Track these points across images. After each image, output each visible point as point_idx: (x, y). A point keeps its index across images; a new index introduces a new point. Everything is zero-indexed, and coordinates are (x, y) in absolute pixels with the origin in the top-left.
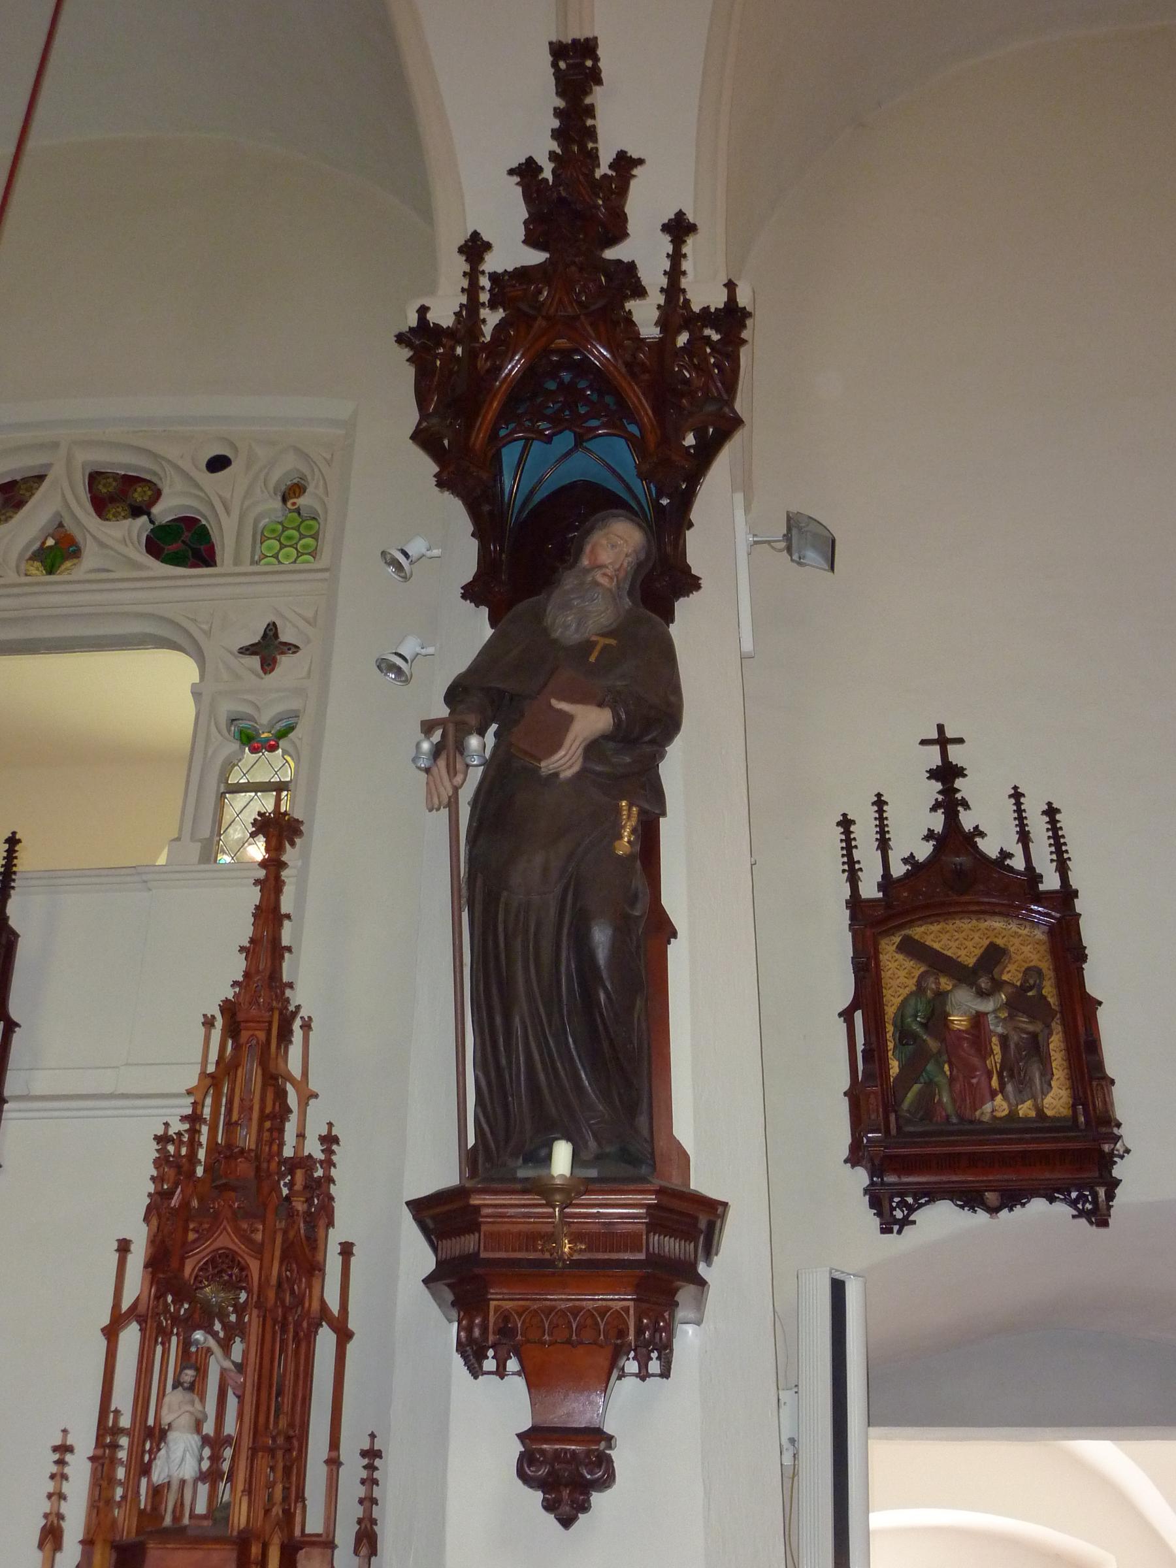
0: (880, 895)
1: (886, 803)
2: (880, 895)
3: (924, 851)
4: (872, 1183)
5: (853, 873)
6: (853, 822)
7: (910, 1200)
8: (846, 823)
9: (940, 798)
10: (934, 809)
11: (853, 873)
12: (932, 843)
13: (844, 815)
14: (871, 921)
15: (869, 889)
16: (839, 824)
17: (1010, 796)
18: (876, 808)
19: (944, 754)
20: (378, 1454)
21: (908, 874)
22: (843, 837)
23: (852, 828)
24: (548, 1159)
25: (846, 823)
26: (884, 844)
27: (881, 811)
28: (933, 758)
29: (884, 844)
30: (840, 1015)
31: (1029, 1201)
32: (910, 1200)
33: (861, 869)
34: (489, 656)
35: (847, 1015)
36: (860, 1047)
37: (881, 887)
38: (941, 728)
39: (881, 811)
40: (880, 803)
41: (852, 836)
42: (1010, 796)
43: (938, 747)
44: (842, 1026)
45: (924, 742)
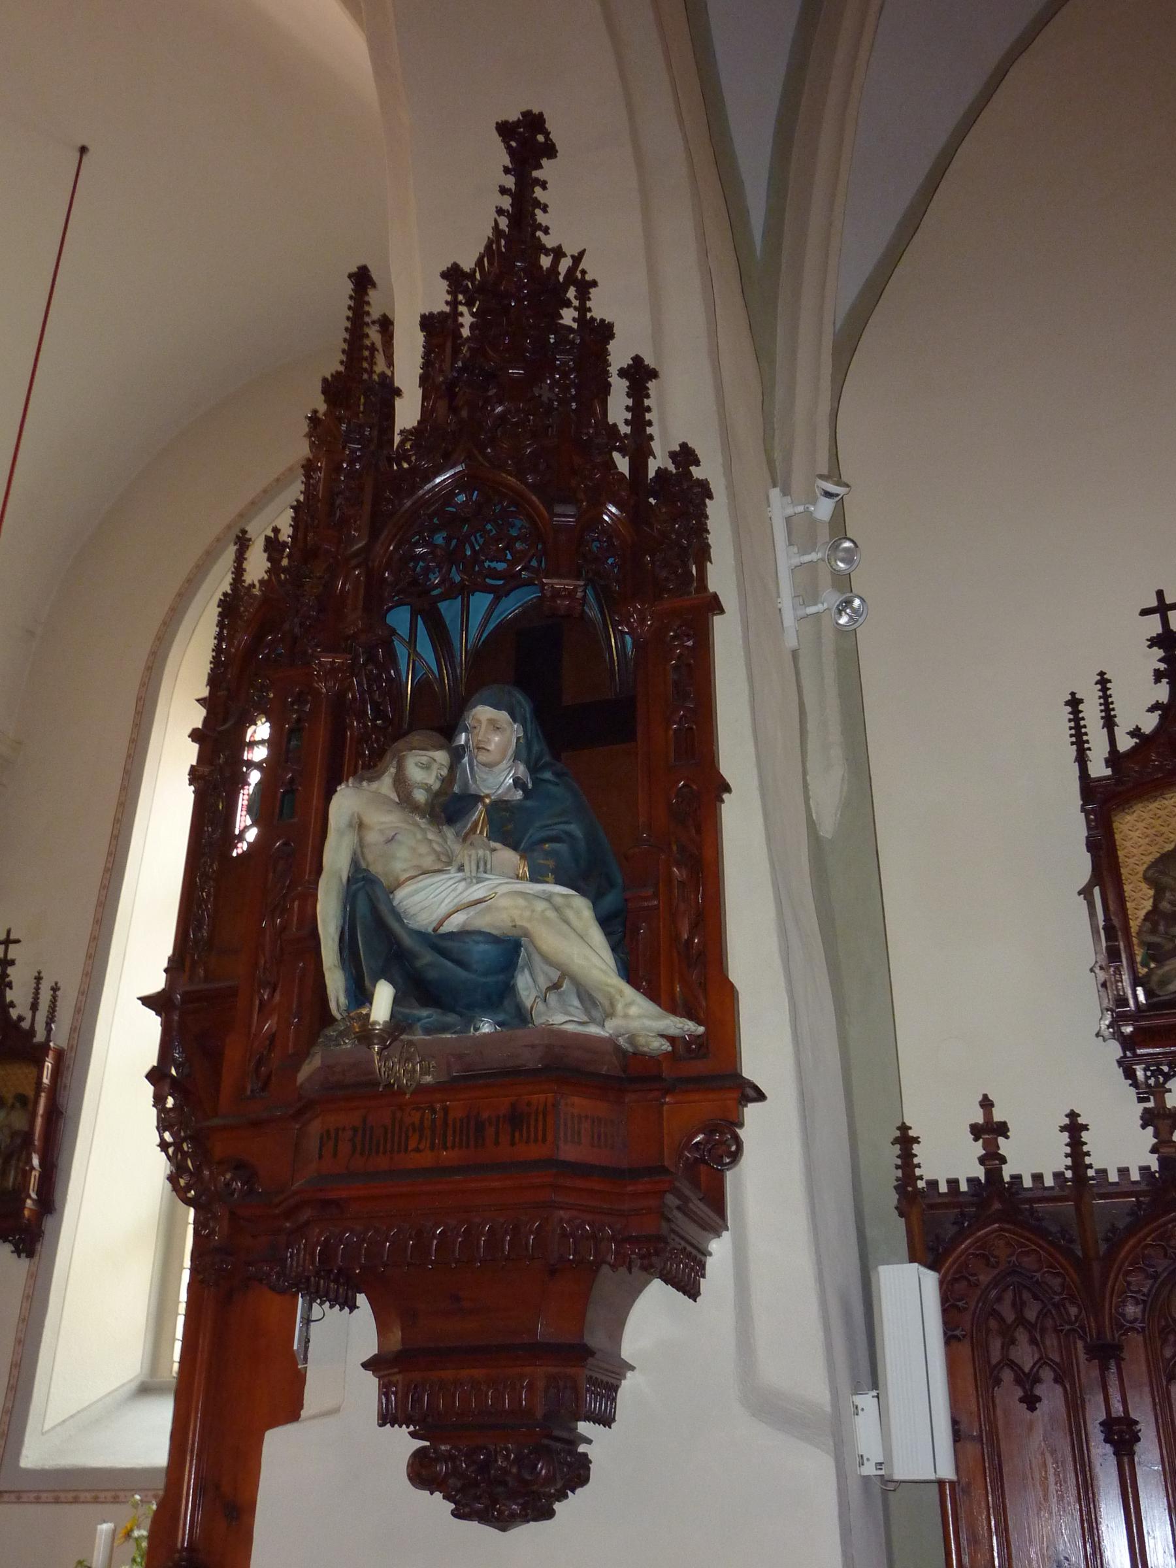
0: (1109, 772)
1: (1110, 681)
2: (1109, 772)
3: (1150, 723)
4: (1125, 1056)
5: (1082, 759)
6: (1081, 701)
7: (1166, 1069)
8: (1074, 703)
9: (1162, 666)
10: (1151, 709)
11: (1082, 759)
12: (1165, 681)
13: (1073, 694)
14: (1103, 801)
15: (1098, 769)
16: (1067, 703)
17: (1063, 1129)
18: (1099, 687)
19: (1165, 622)
20: (1002, 1129)
21: (1134, 749)
22: (1071, 717)
23: (1085, 1136)
24: (172, 1135)
25: (1074, 703)
26: (1109, 722)
27: (1104, 689)
28: (1153, 626)
29: (1109, 722)
30: (1080, 893)
31: (169, 1157)
32: (1166, 1069)
33: (1089, 749)
34: (462, 270)
35: (1086, 892)
36: (1101, 924)
37: (1109, 762)
38: (1160, 594)
39: (1104, 689)
40: (1103, 682)
41: (1081, 715)
42: (1063, 1129)
43: (1158, 615)
44: (1081, 901)
45: (1074, 1128)
